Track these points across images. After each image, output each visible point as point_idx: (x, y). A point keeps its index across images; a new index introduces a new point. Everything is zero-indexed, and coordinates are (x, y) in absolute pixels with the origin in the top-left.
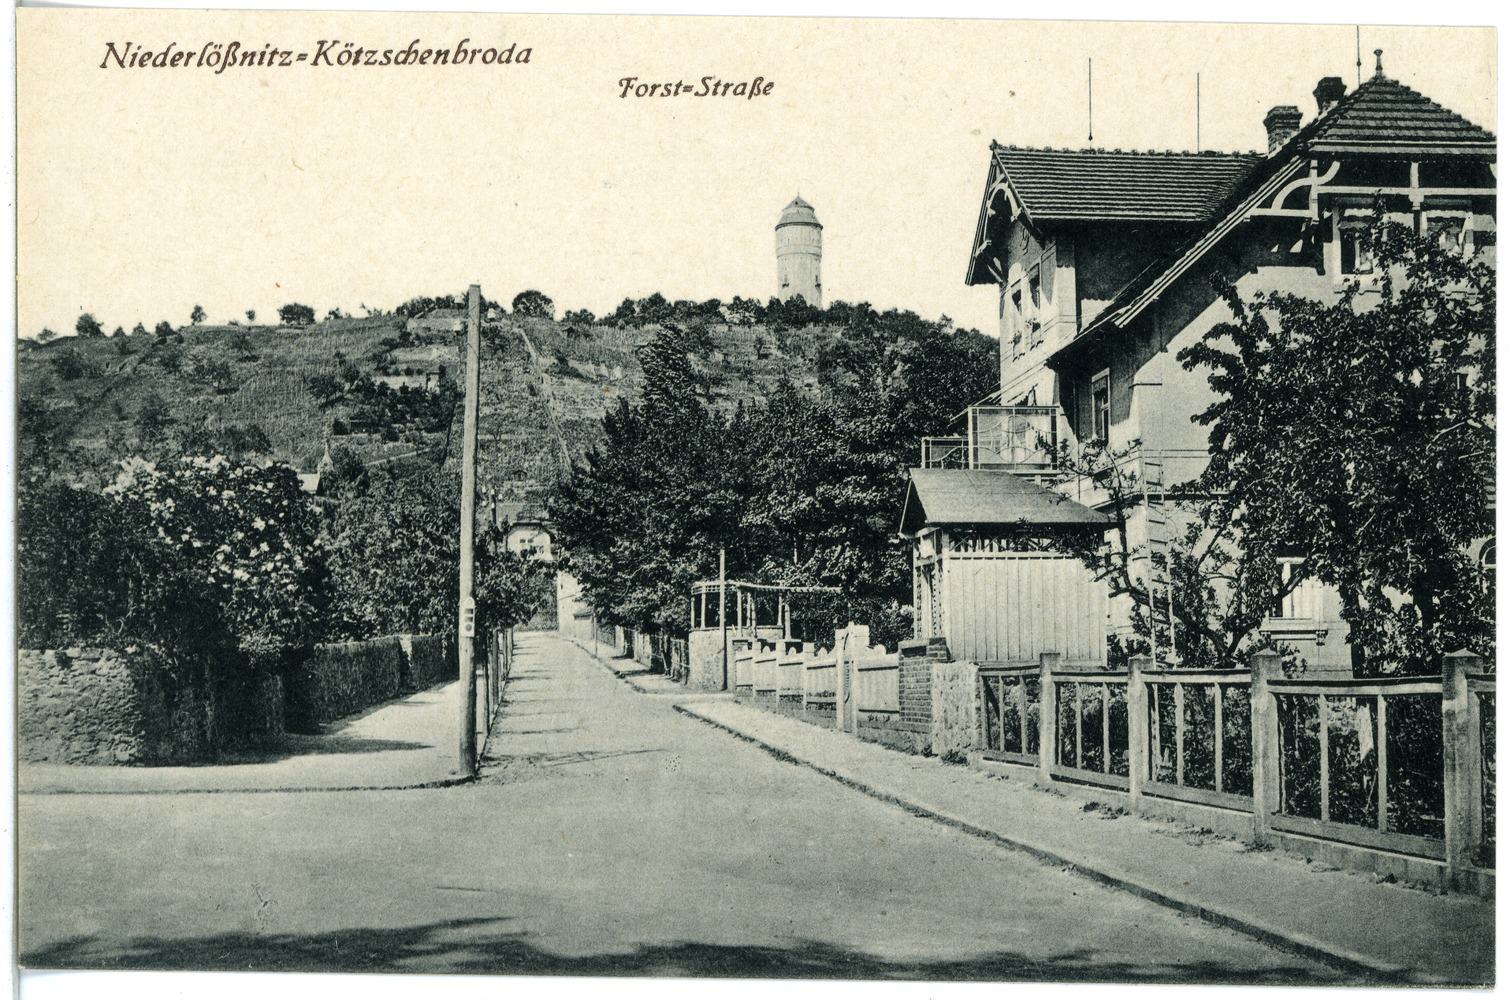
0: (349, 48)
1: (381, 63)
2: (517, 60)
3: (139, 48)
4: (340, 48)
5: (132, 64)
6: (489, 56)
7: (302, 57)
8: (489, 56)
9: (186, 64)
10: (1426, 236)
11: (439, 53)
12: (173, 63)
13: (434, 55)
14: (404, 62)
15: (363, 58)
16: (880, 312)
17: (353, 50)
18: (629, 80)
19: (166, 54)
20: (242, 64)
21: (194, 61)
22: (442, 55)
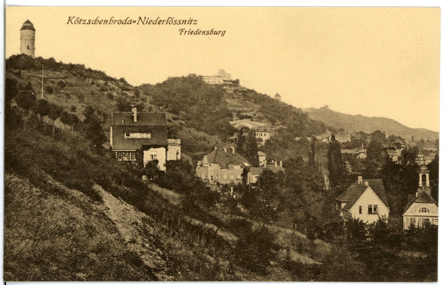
0: (172, 19)
1: (88, 24)
3: (148, 18)
5: (146, 24)
7: (135, 22)
9: (163, 24)
10: (216, 205)
11: (183, 21)
12: (159, 23)
13: (104, 21)
14: (95, 23)
15: (82, 22)
17: (79, 20)
18: (182, 29)
20: (182, 24)
21: (165, 22)
22: (106, 21)
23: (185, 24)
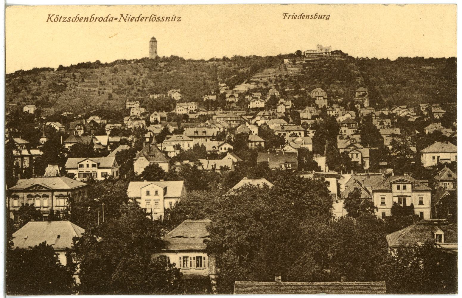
2: (109, 21)
3: (131, 15)
4: (55, 16)
5: (128, 21)
6: (101, 19)
7: (116, 19)
8: (101, 19)
11: (167, 18)
13: (84, 19)
15: (62, 20)
16: (185, 59)
17: (59, 18)
19: (139, 18)
20: (166, 21)
21: (148, 19)
22: (86, 19)
23: (169, 21)
